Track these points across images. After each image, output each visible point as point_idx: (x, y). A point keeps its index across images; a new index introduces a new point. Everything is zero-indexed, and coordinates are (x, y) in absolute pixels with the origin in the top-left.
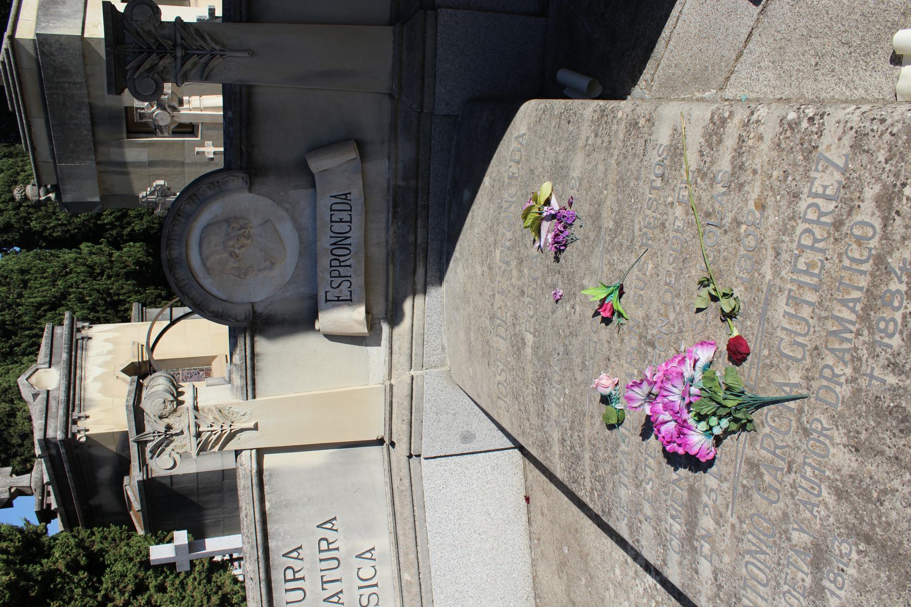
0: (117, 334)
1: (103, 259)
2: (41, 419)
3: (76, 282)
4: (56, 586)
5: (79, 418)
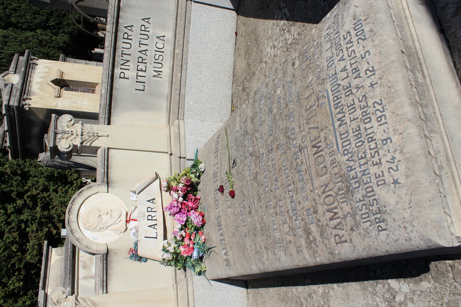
0: (50, 65)
1: (48, 38)
2: (7, 96)
3: (32, 47)
4: (5, 179)
5: (27, 99)
